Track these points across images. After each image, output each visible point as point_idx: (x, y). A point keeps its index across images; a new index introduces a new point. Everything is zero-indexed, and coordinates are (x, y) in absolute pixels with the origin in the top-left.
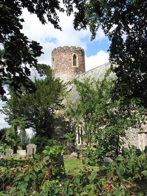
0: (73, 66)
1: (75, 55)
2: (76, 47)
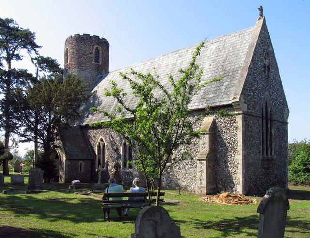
0: (93, 62)
1: (97, 48)
2: (101, 38)
